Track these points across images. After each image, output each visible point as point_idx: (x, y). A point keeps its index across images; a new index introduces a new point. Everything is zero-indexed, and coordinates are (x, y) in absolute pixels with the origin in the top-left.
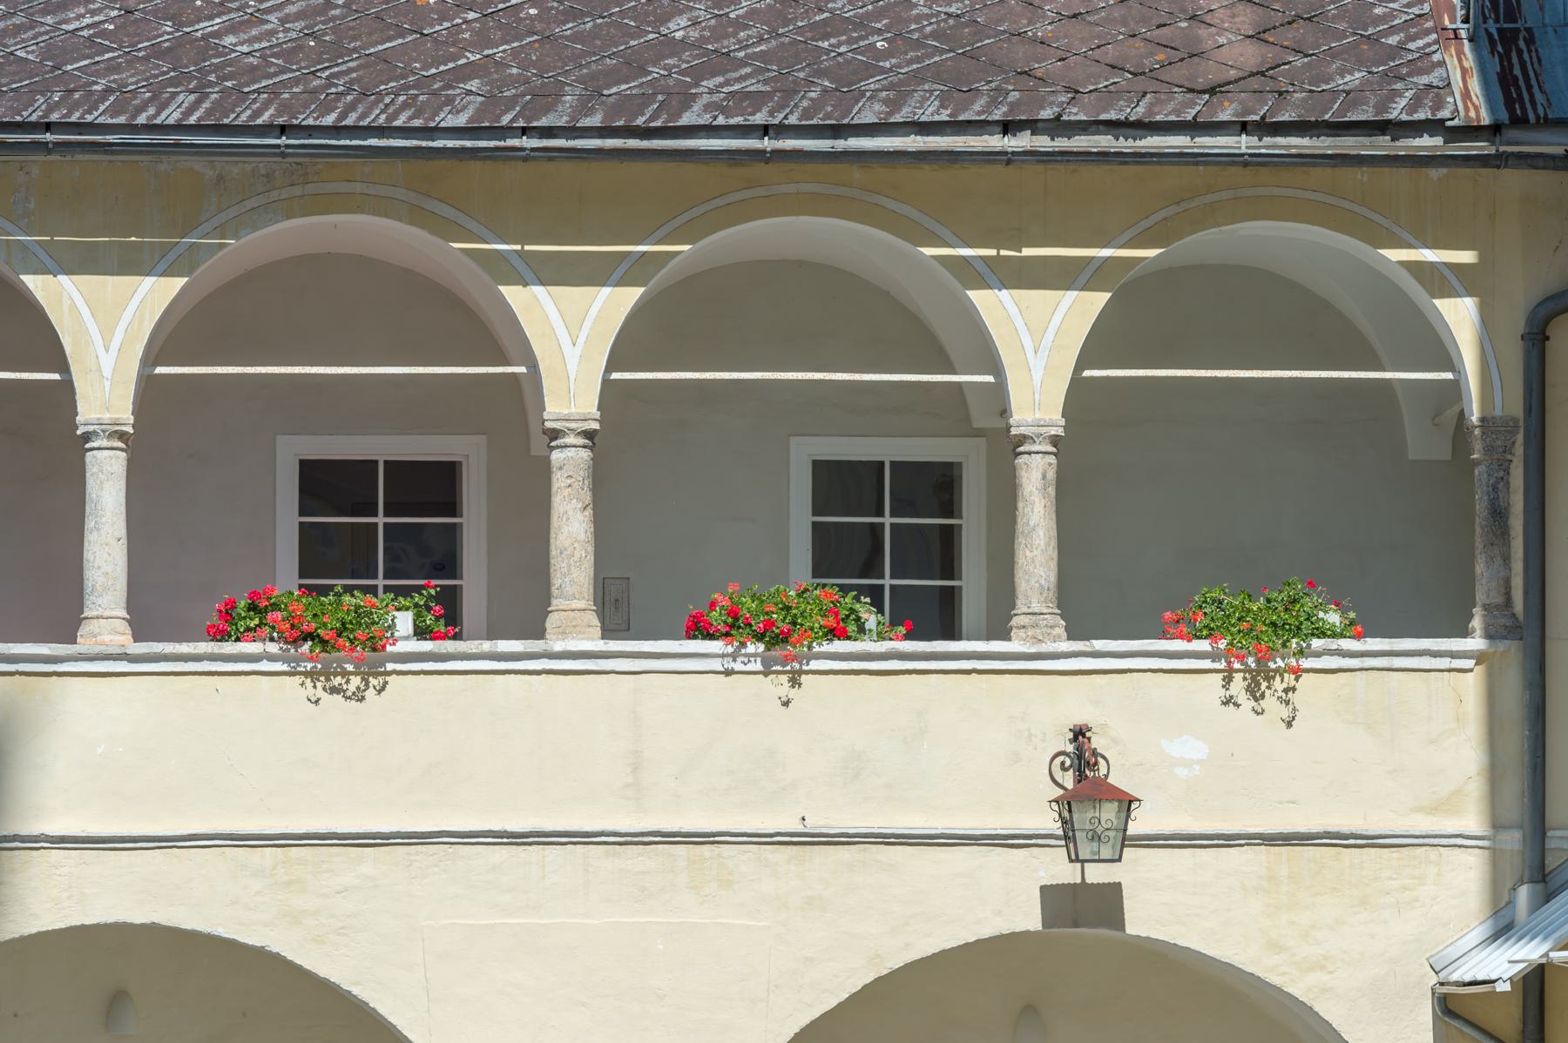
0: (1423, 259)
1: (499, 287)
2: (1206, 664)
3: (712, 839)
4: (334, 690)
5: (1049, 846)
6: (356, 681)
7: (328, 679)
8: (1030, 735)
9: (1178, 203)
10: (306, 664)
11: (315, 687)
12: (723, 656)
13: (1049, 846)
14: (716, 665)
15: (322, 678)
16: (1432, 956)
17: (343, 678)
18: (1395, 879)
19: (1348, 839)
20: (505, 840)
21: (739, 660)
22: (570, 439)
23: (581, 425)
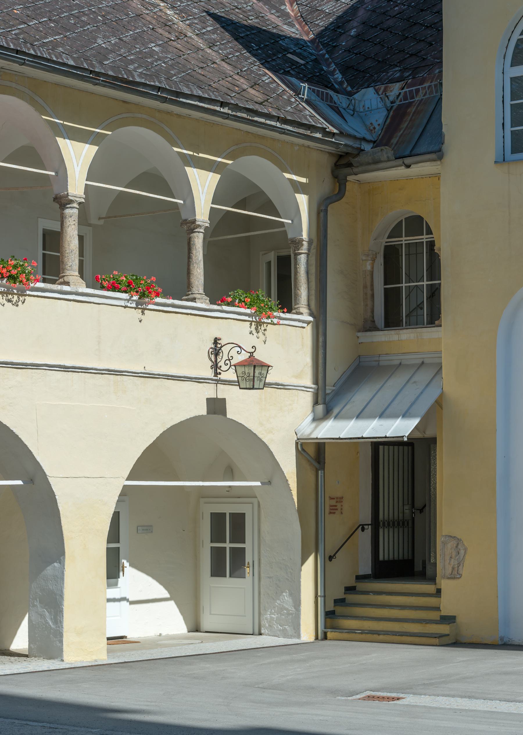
0: (293, 178)
1: (56, 138)
2: (247, 318)
3: (122, 373)
4: (9, 301)
5: (209, 383)
6: (16, 297)
7: (7, 296)
8: (203, 340)
9: (237, 145)
10: (2, 288)
11: (3, 299)
12: (125, 300)
13: (209, 383)
14: (122, 303)
15: (5, 295)
16: (296, 429)
17: (12, 296)
18: (288, 401)
19: (279, 386)
20: (62, 369)
21: (130, 302)
22: (75, 205)
23: (80, 200)
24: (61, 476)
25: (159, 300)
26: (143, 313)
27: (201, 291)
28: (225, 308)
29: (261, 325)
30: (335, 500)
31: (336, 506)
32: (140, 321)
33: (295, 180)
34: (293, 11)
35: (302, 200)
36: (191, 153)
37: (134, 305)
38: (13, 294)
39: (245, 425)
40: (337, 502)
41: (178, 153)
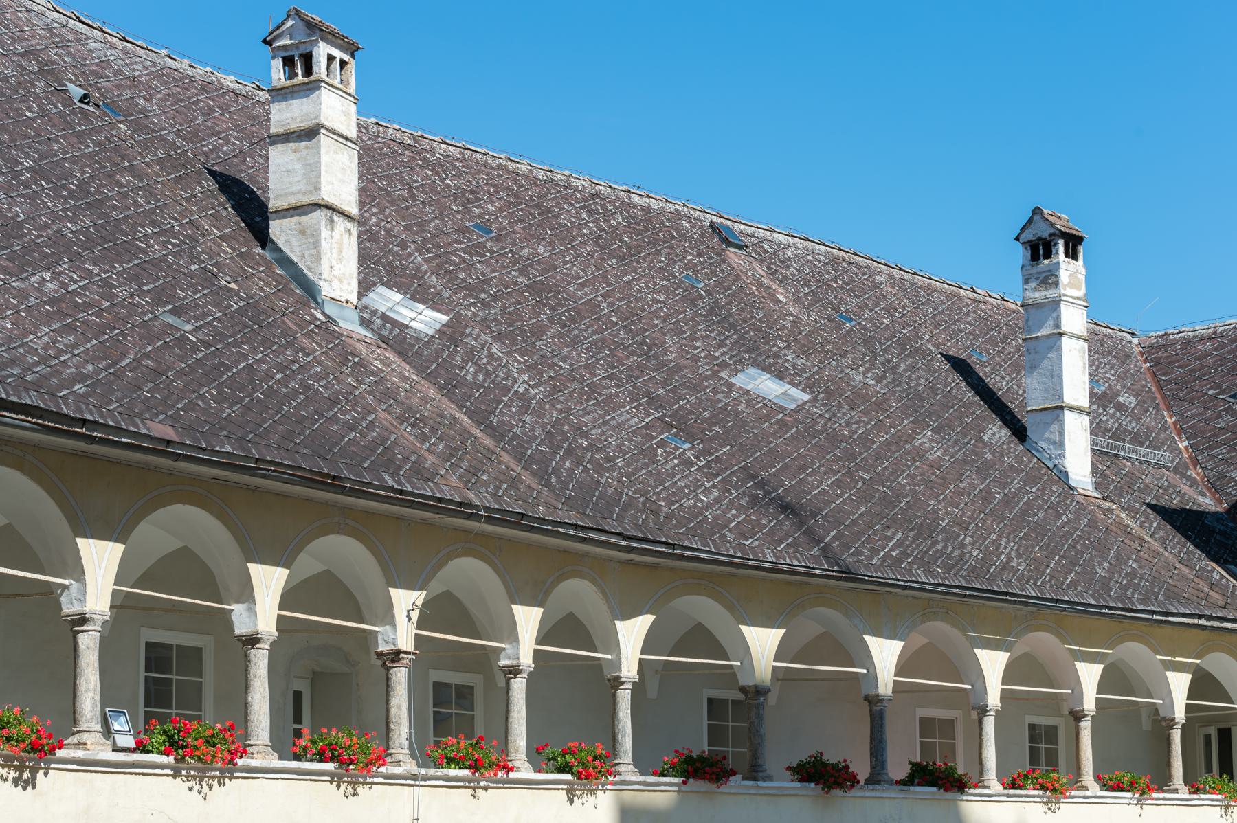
2: (1218, 803)
4: (1049, 809)
14: (1127, 801)
22: (1089, 718)
25: (1155, 795)
27: (1181, 782)
28: (1203, 796)
34: (1198, 474)
36: (1169, 658)
37: (1135, 802)
38: (1052, 803)
41: (1160, 660)
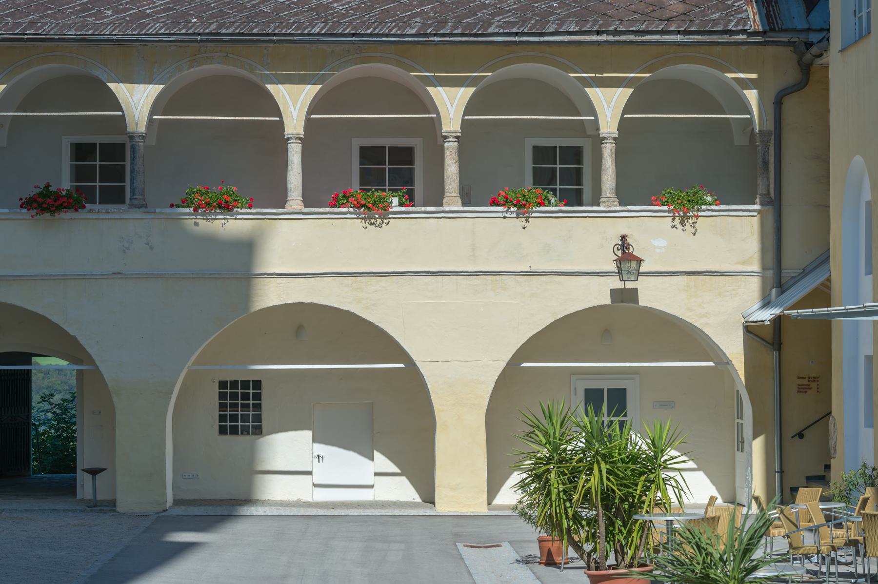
2: (666, 214)
4: (372, 224)
5: (613, 276)
6: (379, 221)
7: (370, 220)
11: (365, 223)
12: (503, 212)
13: (613, 276)
14: (501, 215)
15: (368, 220)
24: (430, 360)
26: (527, 221)
29: (689, 219)
30: (807, 379)
31: (809, 385)
32: (524, 228)
33: (743, 78)
35: (752, 96)
39: (50, 317)
40: (809, 381)
